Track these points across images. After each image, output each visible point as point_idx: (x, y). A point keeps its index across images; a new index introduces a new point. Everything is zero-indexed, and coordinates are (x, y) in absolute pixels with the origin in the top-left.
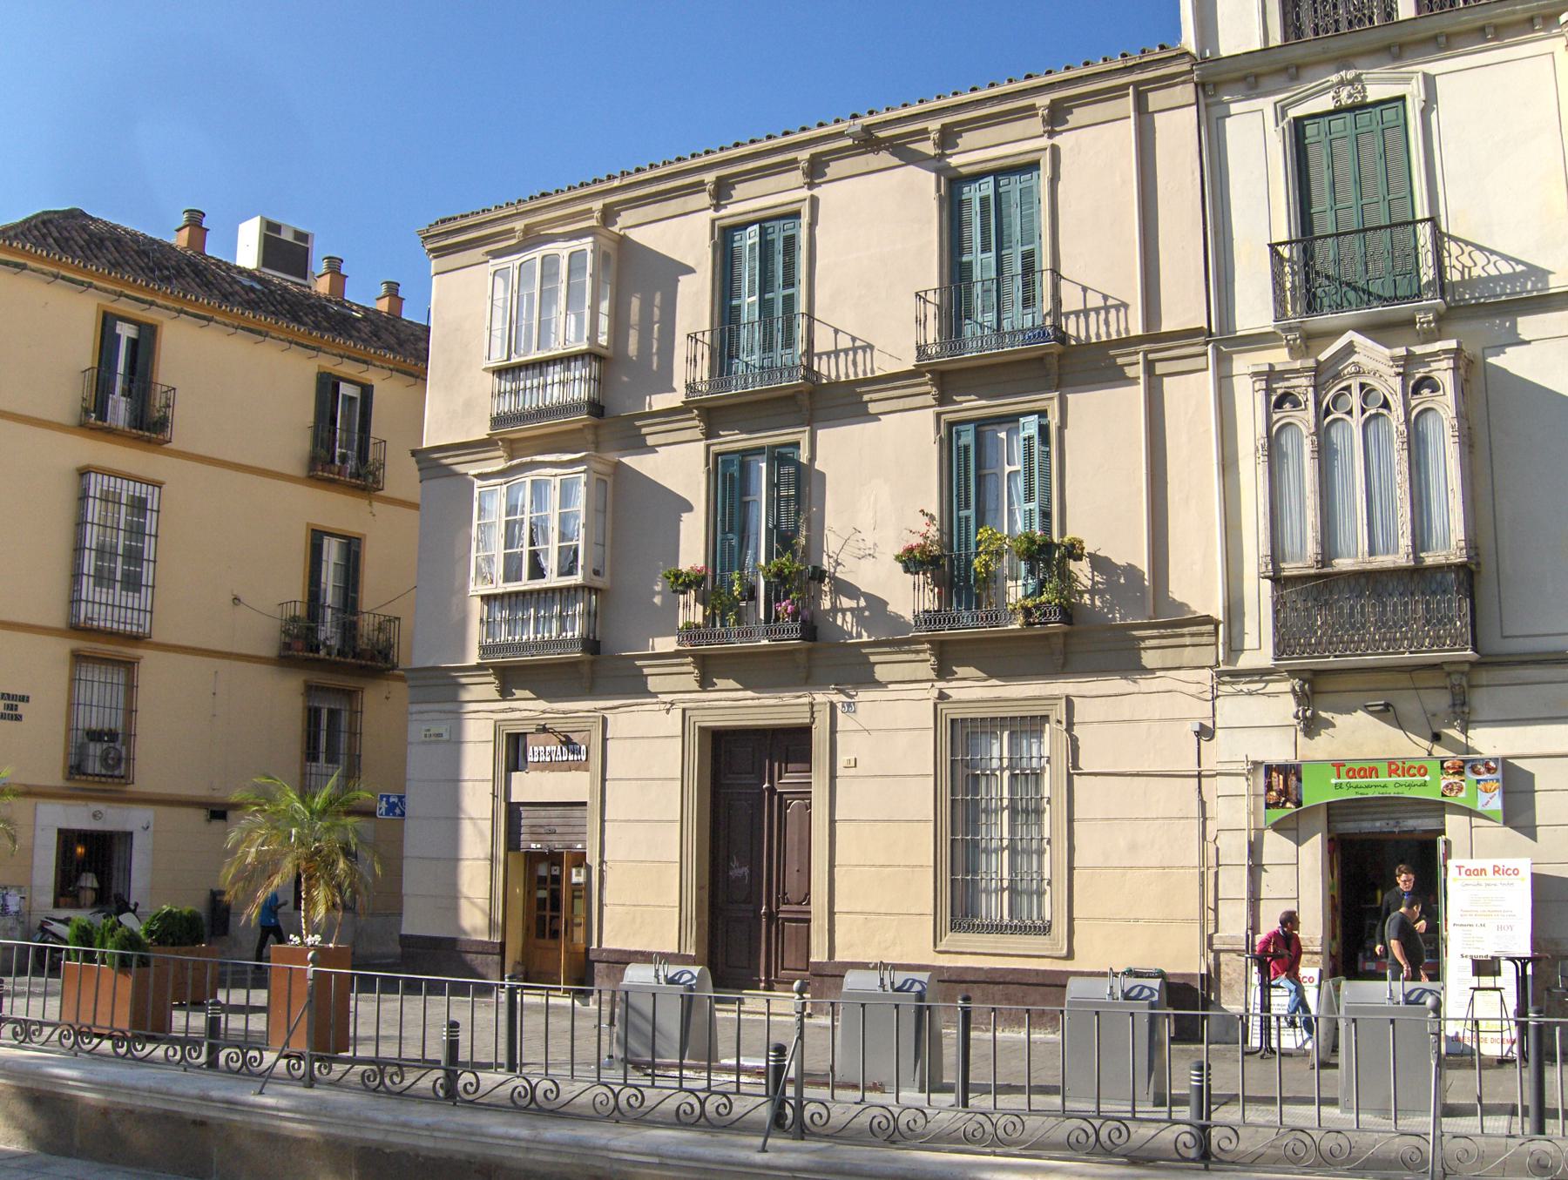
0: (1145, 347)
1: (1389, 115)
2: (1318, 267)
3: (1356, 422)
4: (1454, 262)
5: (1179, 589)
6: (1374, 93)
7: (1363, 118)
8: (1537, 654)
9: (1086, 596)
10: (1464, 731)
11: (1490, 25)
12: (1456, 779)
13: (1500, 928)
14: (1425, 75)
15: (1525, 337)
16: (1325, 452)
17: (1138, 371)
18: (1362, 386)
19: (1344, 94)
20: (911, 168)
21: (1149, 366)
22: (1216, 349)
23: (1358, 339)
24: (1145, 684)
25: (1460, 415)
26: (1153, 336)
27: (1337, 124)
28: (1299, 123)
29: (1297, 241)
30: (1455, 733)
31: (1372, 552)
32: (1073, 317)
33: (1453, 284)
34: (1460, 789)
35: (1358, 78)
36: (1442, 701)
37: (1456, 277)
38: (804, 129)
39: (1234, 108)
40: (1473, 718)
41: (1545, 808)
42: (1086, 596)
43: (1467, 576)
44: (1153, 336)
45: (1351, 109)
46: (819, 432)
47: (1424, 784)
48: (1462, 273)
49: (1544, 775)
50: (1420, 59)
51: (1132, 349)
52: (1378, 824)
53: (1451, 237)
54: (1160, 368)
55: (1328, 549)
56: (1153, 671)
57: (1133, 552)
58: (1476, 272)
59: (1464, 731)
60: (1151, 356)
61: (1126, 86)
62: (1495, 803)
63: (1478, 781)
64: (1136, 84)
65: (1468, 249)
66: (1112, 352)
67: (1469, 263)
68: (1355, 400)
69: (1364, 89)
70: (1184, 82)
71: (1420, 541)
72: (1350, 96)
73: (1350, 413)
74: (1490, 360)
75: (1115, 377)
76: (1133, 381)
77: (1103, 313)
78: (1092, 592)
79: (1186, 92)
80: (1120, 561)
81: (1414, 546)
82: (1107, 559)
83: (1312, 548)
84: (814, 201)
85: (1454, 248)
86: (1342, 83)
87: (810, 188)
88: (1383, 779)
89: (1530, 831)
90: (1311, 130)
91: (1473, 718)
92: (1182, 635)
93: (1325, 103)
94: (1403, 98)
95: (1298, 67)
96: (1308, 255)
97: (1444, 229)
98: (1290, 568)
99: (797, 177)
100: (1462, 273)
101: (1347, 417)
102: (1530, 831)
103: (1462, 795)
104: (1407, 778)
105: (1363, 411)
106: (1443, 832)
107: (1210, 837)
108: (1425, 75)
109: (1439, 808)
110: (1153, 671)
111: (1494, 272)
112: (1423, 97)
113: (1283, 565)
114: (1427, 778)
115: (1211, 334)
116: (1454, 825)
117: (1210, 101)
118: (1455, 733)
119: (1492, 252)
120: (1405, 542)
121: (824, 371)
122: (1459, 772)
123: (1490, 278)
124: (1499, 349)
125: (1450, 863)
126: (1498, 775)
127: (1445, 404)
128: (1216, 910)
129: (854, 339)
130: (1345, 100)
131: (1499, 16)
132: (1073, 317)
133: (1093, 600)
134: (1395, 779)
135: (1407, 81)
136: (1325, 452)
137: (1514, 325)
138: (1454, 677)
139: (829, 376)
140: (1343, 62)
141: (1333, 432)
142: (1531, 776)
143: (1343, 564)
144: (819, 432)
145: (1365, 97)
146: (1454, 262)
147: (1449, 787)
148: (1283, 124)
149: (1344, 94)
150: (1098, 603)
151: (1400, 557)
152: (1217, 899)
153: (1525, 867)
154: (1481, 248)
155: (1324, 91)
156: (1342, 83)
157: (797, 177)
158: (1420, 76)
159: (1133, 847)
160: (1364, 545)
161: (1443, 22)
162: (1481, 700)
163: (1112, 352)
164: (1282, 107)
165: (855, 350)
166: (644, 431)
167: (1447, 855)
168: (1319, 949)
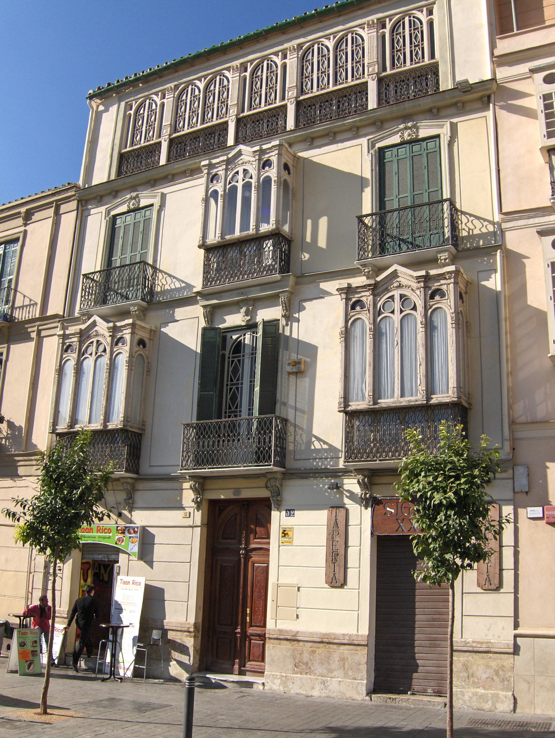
0: (38, 323)
1: (431, 145)
2: (389, 232)
3: (397, 318)
4: (464, 226)
5: (35, 439)
6: (423, 133)
7: (416, 148)
8: (162, 475)
9: (4, 440)
10: (130, 512)
11: (188, 169)
12: (121, 536)
13: (131, 611)
14: (451, 123)
15: (177, 318)
16: (378, 335)
17: (34, 335)
18: (402, 296)
19: (406, 135)
20: (306, 157)
21: (39, 332)
22: (62, 324)
23: (401, 270)
24: (19, 483)
25: (458, 313)
26: (44, 318)
27: (402, 151)
28: (382, 151)
29: (103, 271)
30: (126, 512)
31: (402, 395)
32: (18, 309)
33: (157, 292)
34: (123, 541)
35: (137, 196)
36: (122, 496)
37: (465, 234)
38: (22, 198)
39: (92, 211)
40: (134, 506)
41: (158, 552)
42: (4, 440)
43: (460, 411)
44: (44, 318)
45: (410, 142)
46: (12, 346)
47: (109, 538)
48: (469, 232)
49: (160, 536)
50: (162, 186)
51: (33, 324)
52: (100, 557)
53: (462, 213)
54: (43, 333)
55: (74, 420)
56: (21, 477)
57: (20, 421)
58: (167, 287)
59: (130, 512)
60: (40, 328)
61: (52, 203)
62: (136, 549)
63: (130, 537)
64: (57, 201)
65: (471, 219)
66: (26, 326)
67: (165, 283)
68: (397, 305)
69: (139, 201)
70: (73, 200)
71: (430, 390)
72: (409, 135)
73: (393, 312)
74: (162, 329)
75: (25, 337)
76: (32, 339)
77: (28, 307)
78: (6, 438)
79: (73, 205)
80: (17, 424)
81: (427, 390)
82: (13, 423)
83: (368, 390)
84: (25, 232)
85: (464, 219)
86: (406, 128)
87: (25, 227)
88: (95, 534)
89: (150, 563)
90: (388, 154)
91: (134, 506)
92: (32, 460)
93: (396, 139)
94: (438, 136)
95: (335, 133)
96: (382, 222)
97: (458, 206)
98: (354, 406)
99: (20, 221)
100: (469, 232)
101: (413, 312)
102: (150, 563)
103: (123, 544)
104: (104, 534)
105: (401, 311)
106: (118, 562)
107: (33, 558)
108: (451, 123)
109: (118, 551)
110: (21, 477)
111: (173, 287)
112: (449, 134)
113: (57, 427)
114: (111, 534)
115: (64, 317)
116: (122, 557)
117: (84, 208)
118: (126, 512)
119: (174, 277)
120: (422, 388)
121: (17, 316)
122: (123, 533)
123: (172, 290)
124: (166, 324)
125: (119, 578)
126: (138, 535)
127: (447, 306)
128: (32, 594)
129: (31, 300)
130: (406, 137)
131: (191, 165)
132: (18, 309)
133: (6, 442)
134: (99, 534)
135: (441, 126)
136: (378, 335)
137: (174, 312)
138: (124, 485)
139: (18, 319)
140: (406, 118)
141: (434, 318)
142: (154, 536)
143: (385, 402)
144: (12, 346)
145: (417, 136)
146: (464, 226)
147: (119, 539)
148: (372, 151)
149: (406, 135)
150: (7, 444)
151: (417, 397)
152: (33, 588)
153: (142, 581)
154: (478, 218)
155: (397, 133)
156: (131, 198)
157: (20, 221)
158: (160, 194)
159: (7, 561)
160: (397, 392)
161: (179, 166)
162: (139, 497)
163: (26, 326)
164: (372, 142)
165: (30, 305)
166: (29, 330)
167: (118, 574)
168: (66, 616)
